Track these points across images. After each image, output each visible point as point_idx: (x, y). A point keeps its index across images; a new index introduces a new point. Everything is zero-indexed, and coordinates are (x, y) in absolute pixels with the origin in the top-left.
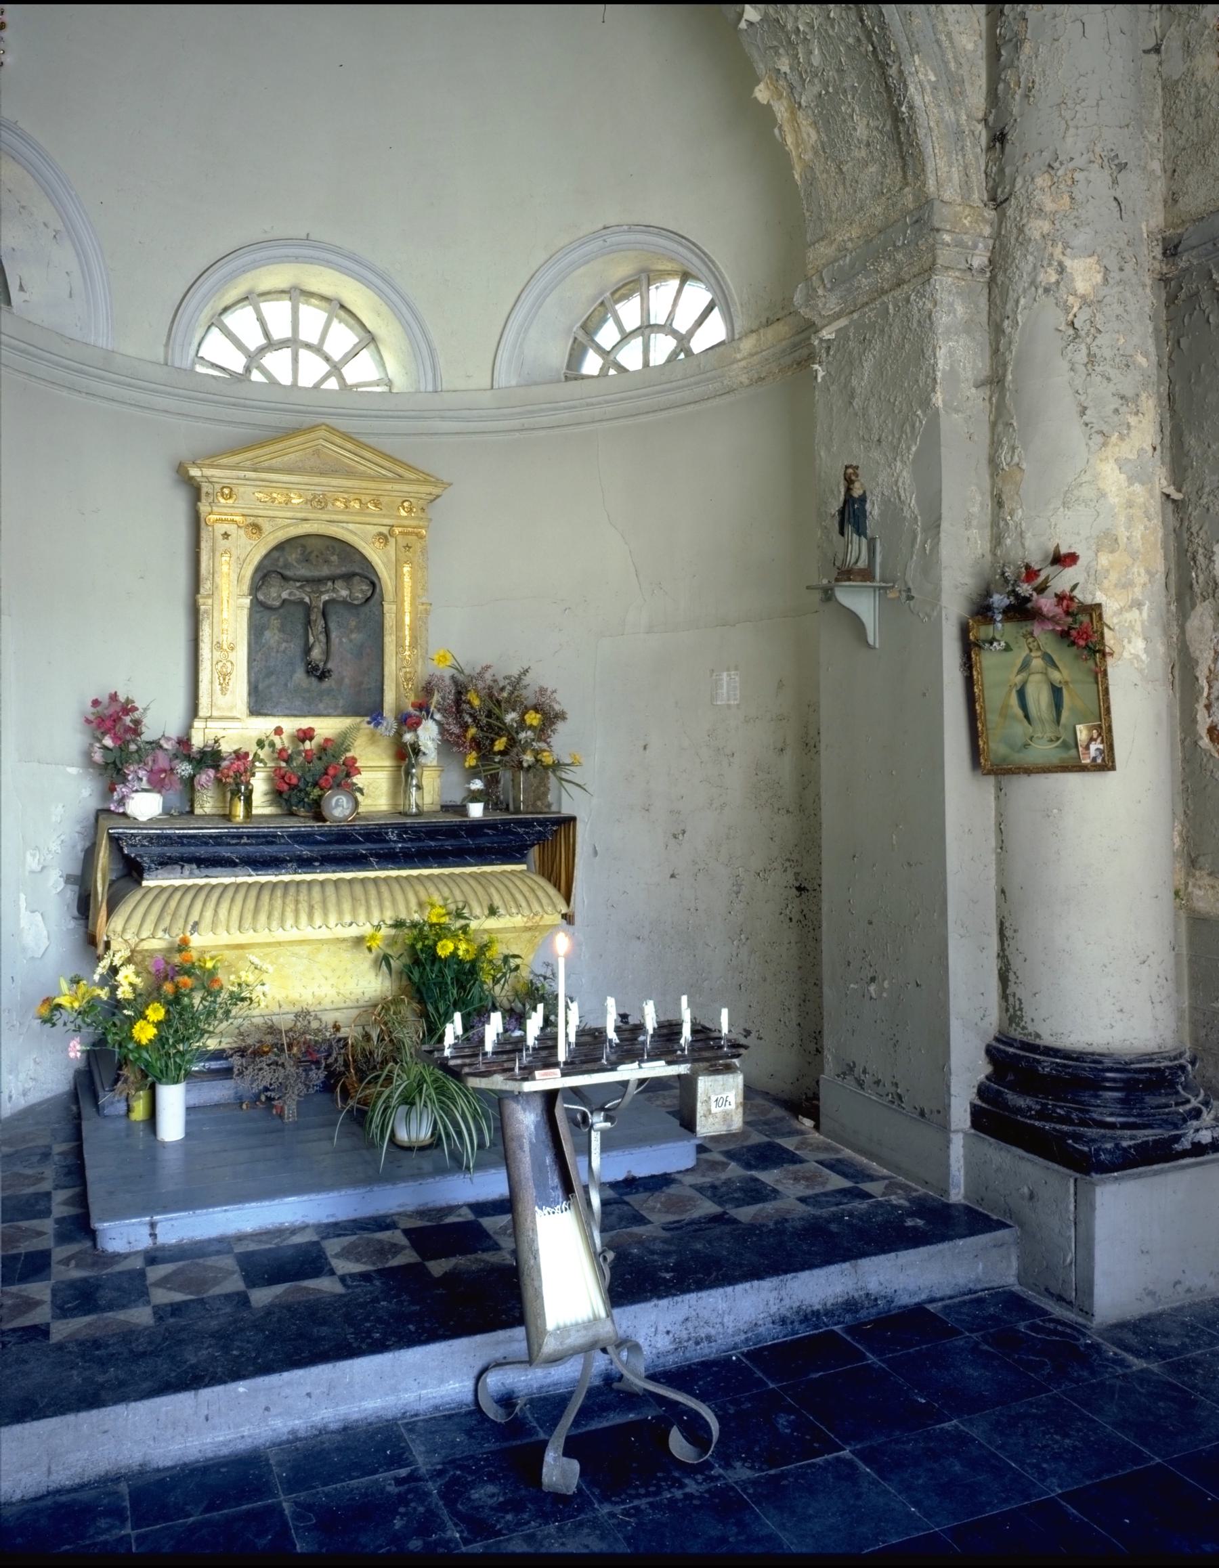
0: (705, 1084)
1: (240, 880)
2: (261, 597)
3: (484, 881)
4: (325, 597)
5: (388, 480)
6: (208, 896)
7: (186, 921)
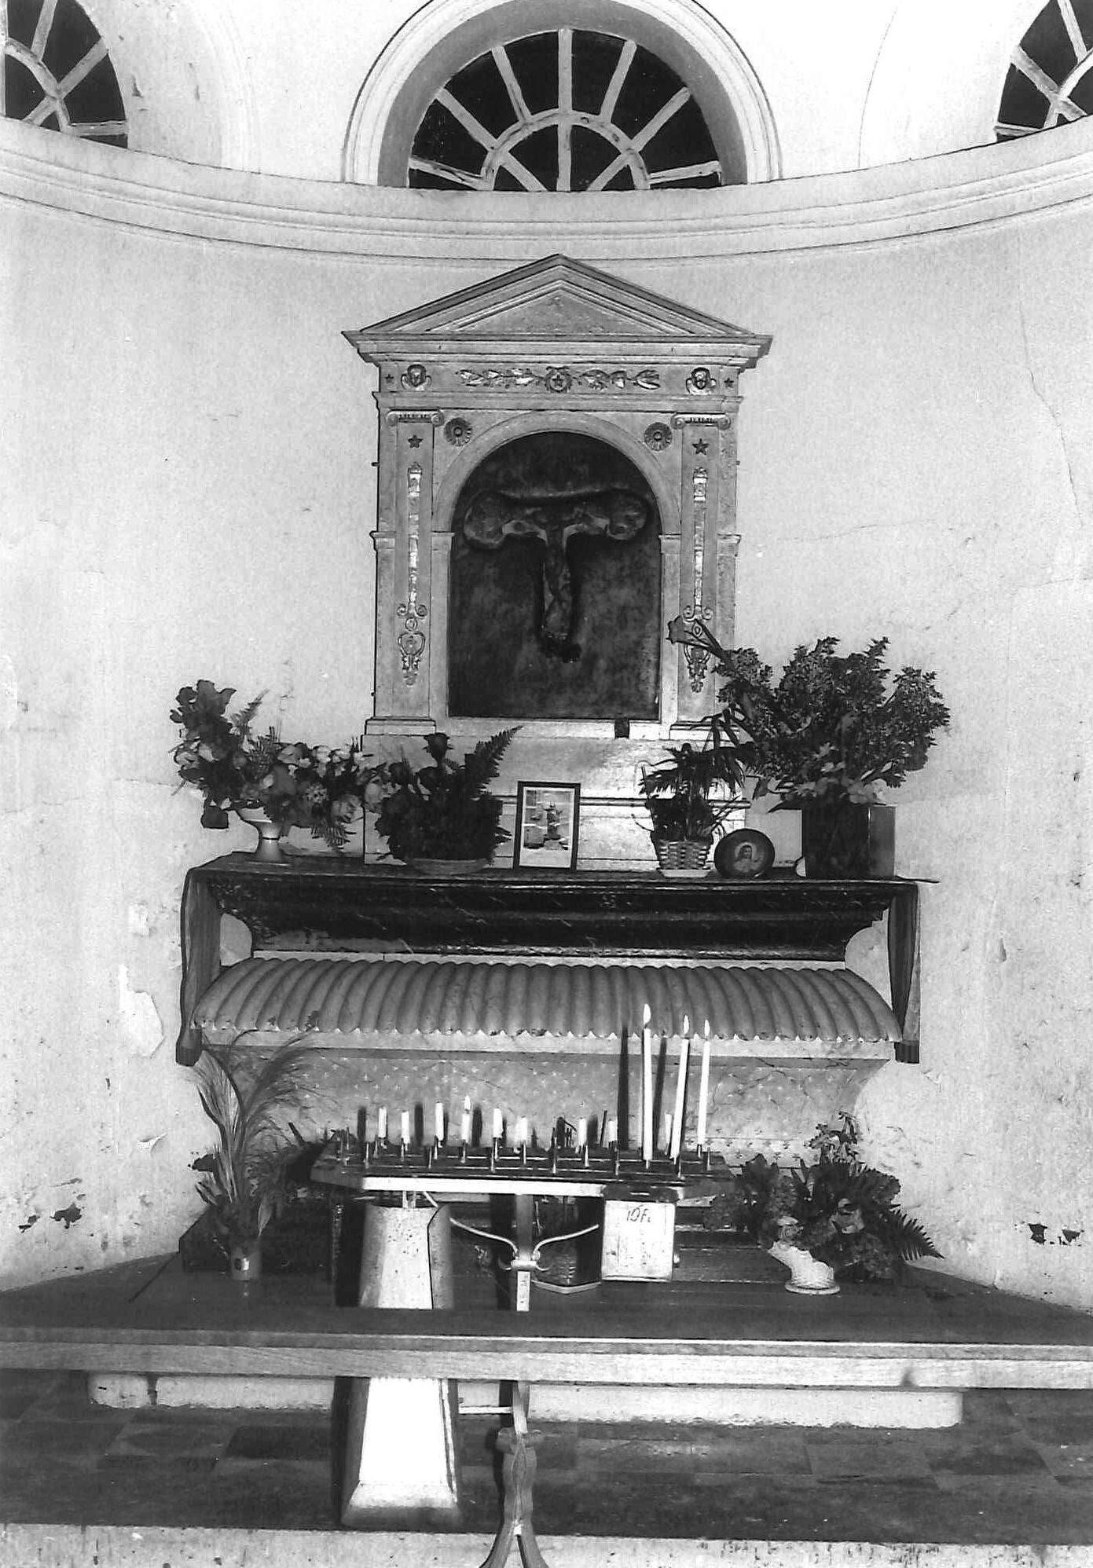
0: (615, 1211)
1: (391, 957)
2: (470, 533)
3: (764, 982)
4: (570, 530)
5: (679, 339)
6: (339, 977)
7: (303, 1011)
